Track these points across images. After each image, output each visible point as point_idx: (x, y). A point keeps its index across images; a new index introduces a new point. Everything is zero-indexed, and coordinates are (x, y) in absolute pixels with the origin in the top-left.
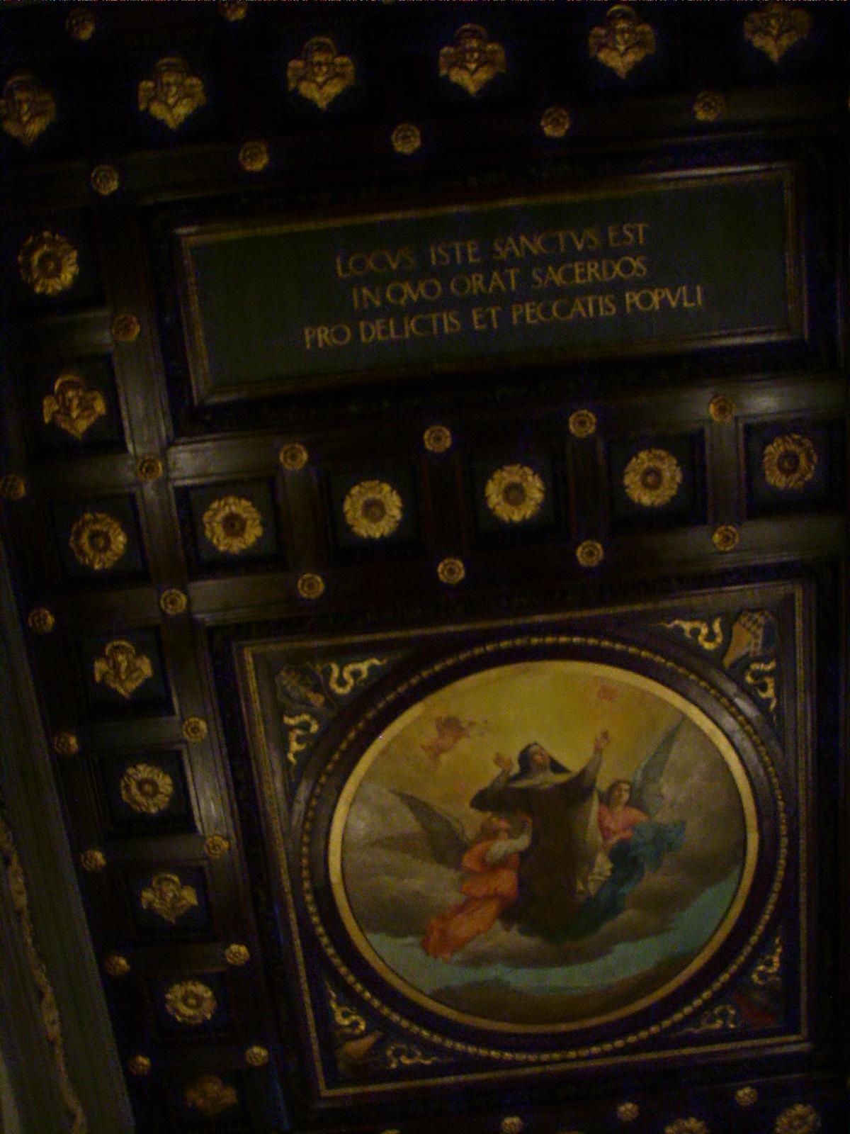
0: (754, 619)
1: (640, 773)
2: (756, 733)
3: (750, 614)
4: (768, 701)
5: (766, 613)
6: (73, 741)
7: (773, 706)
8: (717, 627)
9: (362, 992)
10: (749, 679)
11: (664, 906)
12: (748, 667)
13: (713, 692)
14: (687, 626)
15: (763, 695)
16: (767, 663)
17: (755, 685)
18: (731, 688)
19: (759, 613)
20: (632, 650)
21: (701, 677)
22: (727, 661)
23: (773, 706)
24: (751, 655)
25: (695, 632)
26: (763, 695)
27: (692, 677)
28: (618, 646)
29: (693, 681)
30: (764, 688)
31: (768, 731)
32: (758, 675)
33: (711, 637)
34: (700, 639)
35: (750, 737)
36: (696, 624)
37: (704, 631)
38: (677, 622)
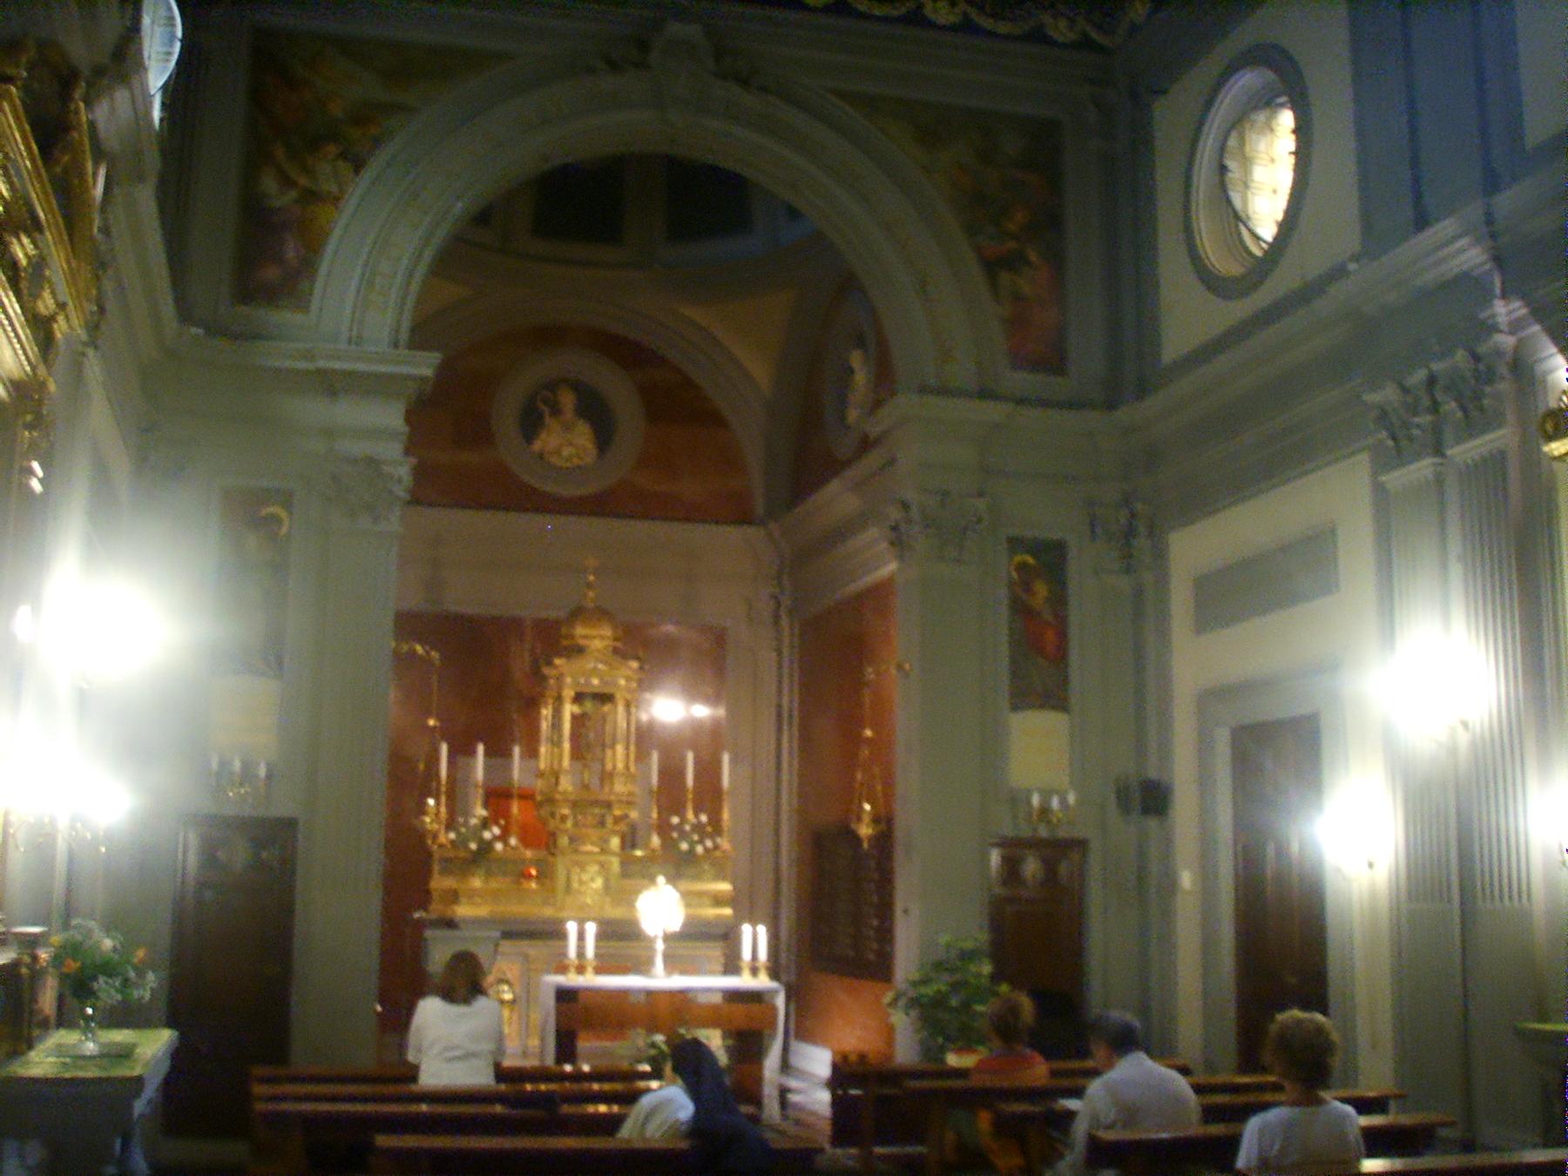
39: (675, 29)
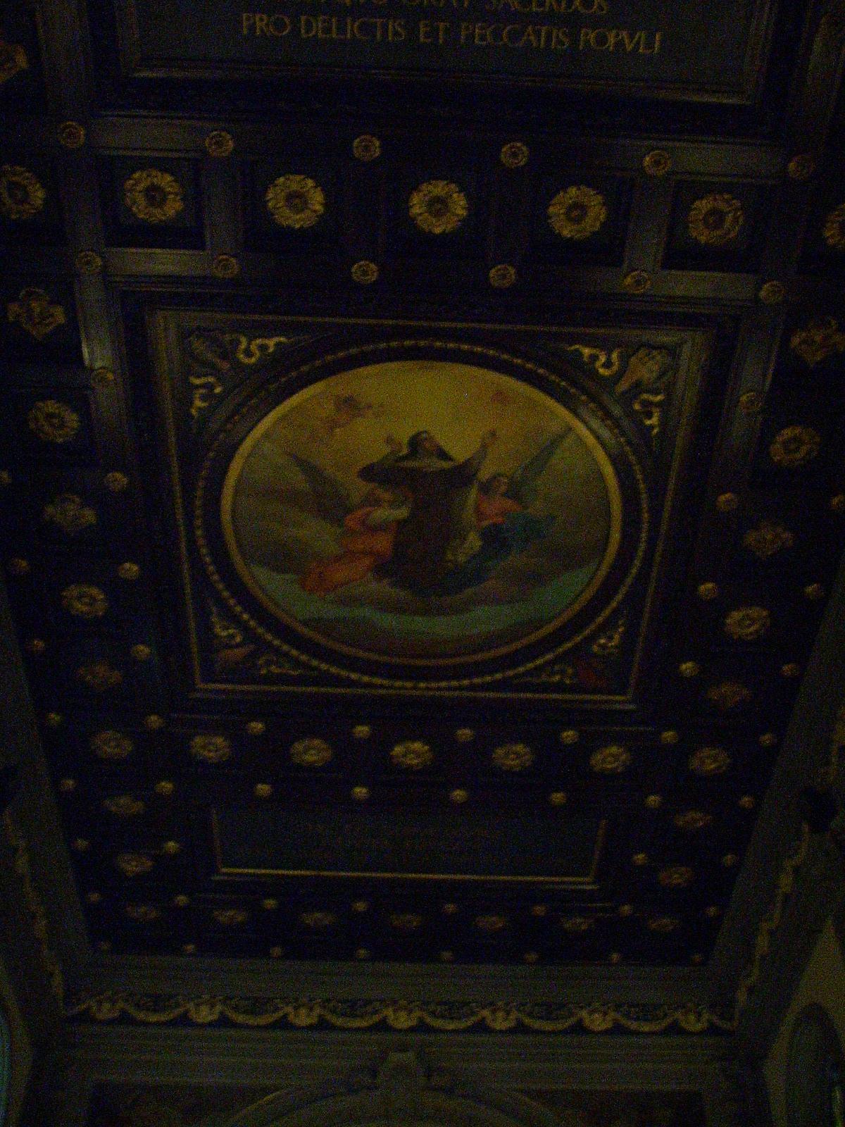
4: (652, 427)
7: (655, 431)
8: (615, 356)
10: (637, 407)
14: (587, 351)
15: (648, 422)
16: (657, 394)
22: (623, 386)
23: (655, 431)
25: (594, 358)
26: (648, 422)
30: (649, 415)
32: (647, 404)
33: (608, 365)
36: (594, 351)
37: (603, 359)
39: (395, 1057)
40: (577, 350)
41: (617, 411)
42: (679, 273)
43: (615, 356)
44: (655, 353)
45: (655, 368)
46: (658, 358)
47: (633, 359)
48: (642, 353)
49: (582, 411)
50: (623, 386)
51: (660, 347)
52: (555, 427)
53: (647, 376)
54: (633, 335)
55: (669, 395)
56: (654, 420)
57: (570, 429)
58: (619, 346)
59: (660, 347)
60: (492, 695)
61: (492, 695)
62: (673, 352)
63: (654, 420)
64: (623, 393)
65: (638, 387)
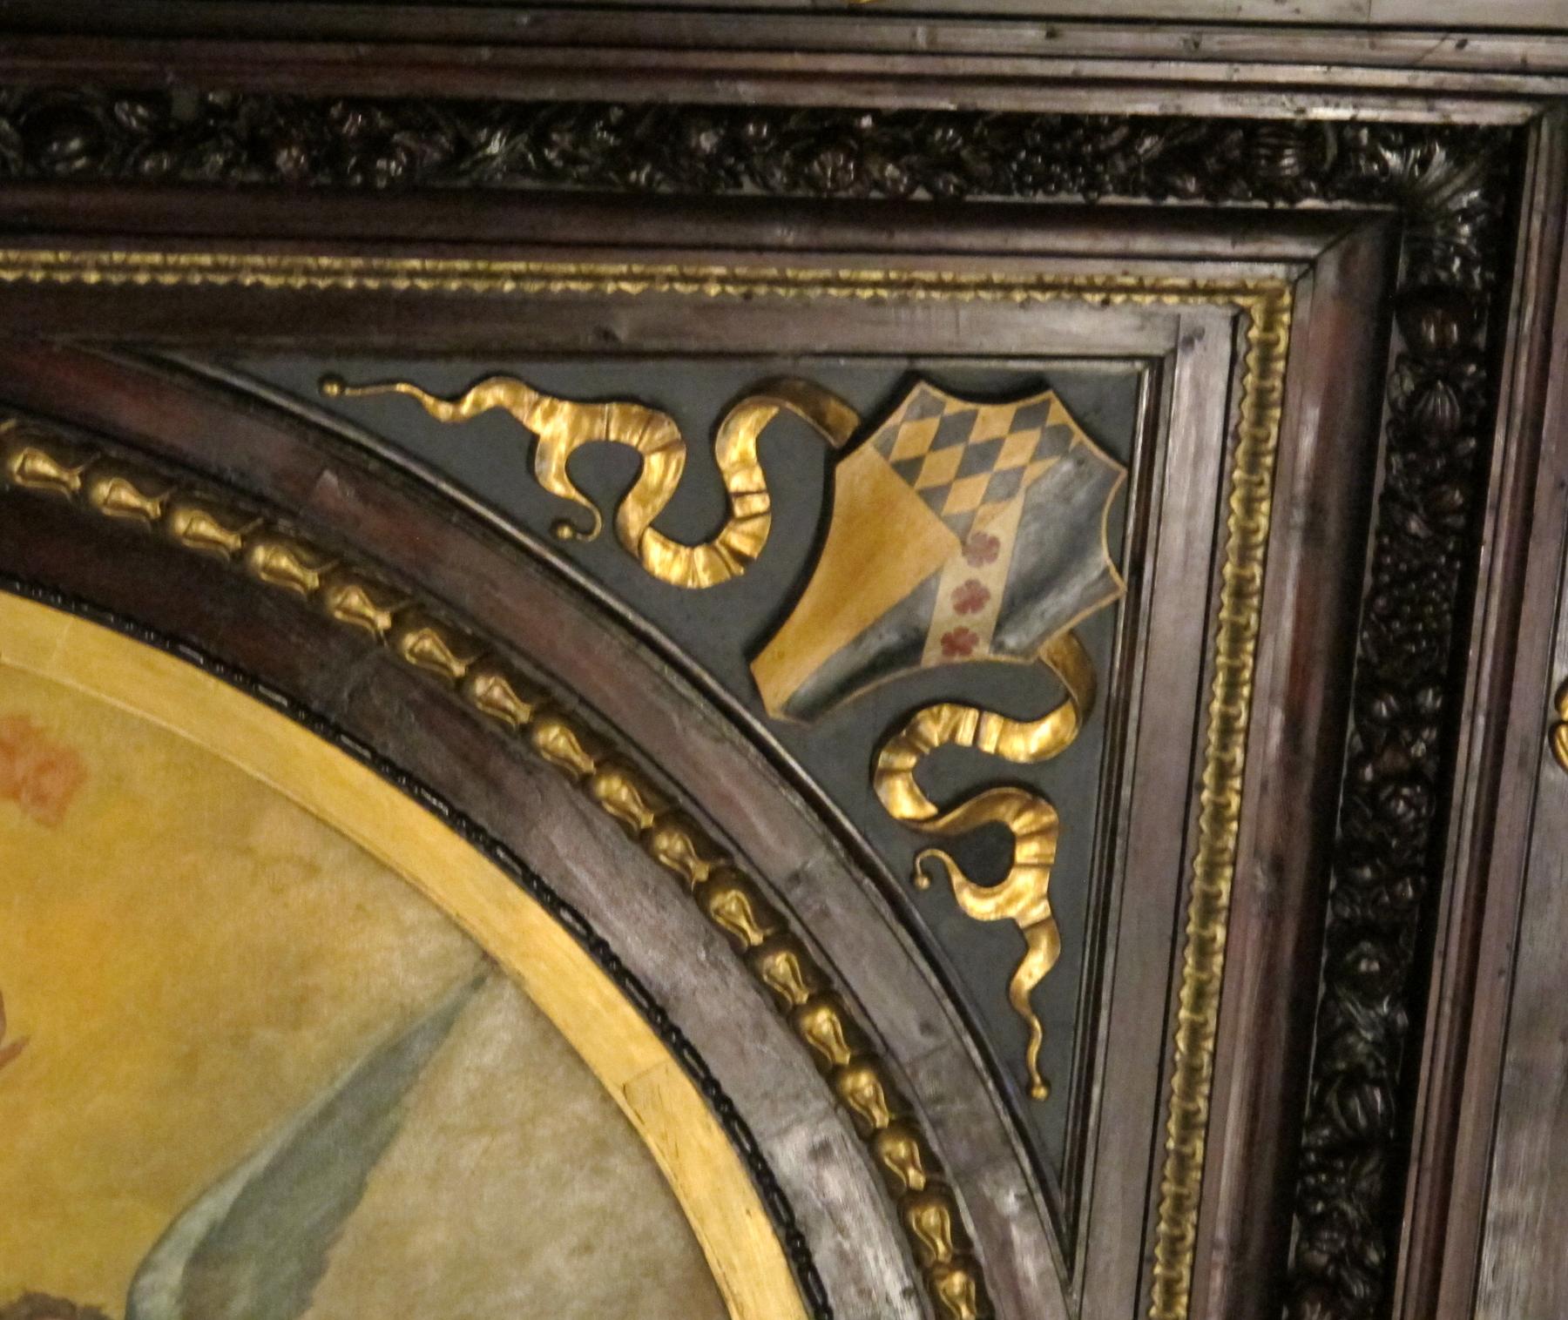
0: (977, 436)
1: (171, 1273)
2: (906, 1124)
3: (954, 406)
4: (1011, 940)
5: (1058, 414)
6: (1457, 495)
7: (1034, 967)
8: (739, 445)
9: (1244, 684)
10: (903, 802)
11: (1255, 877)
12: (899, 728)
13: (671, 844)
14: (556, 428)
15: (979, 905)
16: (1023, 714)
17: (943, 841)
18: (778, 838)
19: (1009, 410)
20: (197, 526)
21: (610, 750)
22: (794, 669)
23: (1034, 967)
24: (932, 656)
25: (610, 472)
26: (979, 905)
27: (555, 738)
28: (117, 495)
29: (563, 768)
30: (990, 860)
31: (924, 1209)
32: (967, 781)
33: (700, 511)
34: (635, 515)
35: (868, 1138)
36: (614, 425)
37: (661, 471)
38: (494, 395)
40: (499, 412)
41: (778, 838)
42: (174, 728)
43: (739, 445)
44: (993, 420)
45: (1004, 524)
46: (1019, 450)
47: (859, 472)
48: (908, 429)
49: (560, 842)
50: (794, 669)
51: (1020, 388)
52: (391, 963)
53: (955, 575)
54: (857, 298)
55: (1106, 712)
56: (1024, 895)
57: (488, 969)
58: (763, 389)
59: (1020, 388)
60: (261, 271)
61: (261, 271)
62: (1118, 419)
63: (1024, 895)
64: (811, 709)
65: (894, 679)
